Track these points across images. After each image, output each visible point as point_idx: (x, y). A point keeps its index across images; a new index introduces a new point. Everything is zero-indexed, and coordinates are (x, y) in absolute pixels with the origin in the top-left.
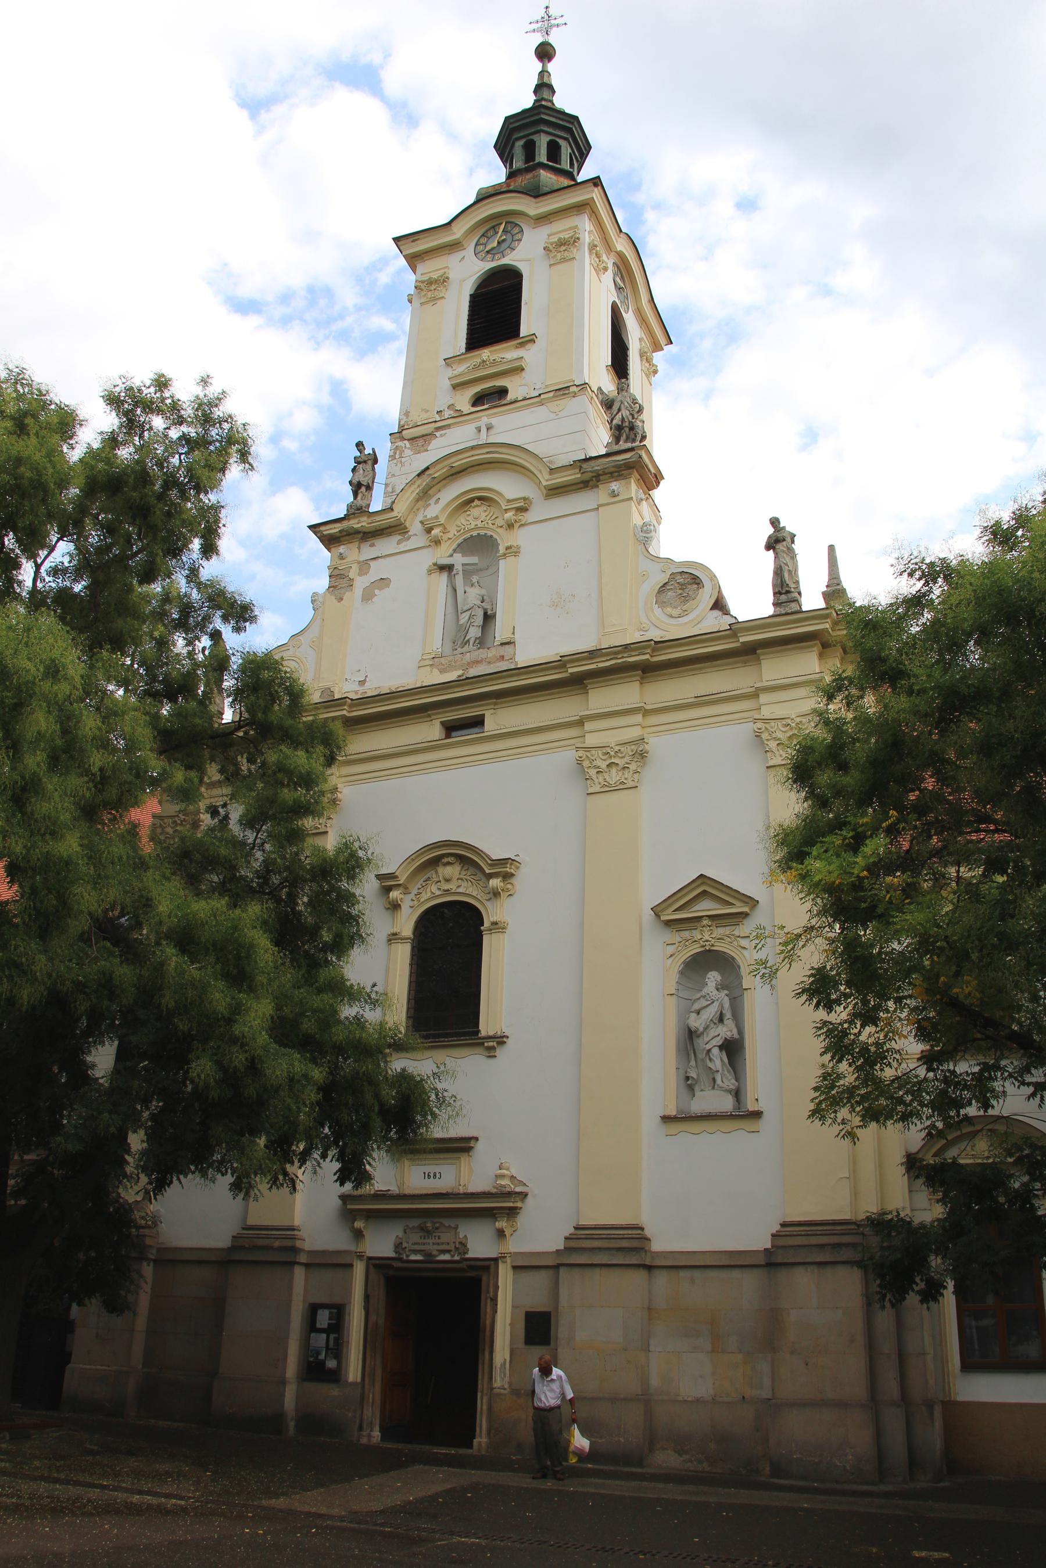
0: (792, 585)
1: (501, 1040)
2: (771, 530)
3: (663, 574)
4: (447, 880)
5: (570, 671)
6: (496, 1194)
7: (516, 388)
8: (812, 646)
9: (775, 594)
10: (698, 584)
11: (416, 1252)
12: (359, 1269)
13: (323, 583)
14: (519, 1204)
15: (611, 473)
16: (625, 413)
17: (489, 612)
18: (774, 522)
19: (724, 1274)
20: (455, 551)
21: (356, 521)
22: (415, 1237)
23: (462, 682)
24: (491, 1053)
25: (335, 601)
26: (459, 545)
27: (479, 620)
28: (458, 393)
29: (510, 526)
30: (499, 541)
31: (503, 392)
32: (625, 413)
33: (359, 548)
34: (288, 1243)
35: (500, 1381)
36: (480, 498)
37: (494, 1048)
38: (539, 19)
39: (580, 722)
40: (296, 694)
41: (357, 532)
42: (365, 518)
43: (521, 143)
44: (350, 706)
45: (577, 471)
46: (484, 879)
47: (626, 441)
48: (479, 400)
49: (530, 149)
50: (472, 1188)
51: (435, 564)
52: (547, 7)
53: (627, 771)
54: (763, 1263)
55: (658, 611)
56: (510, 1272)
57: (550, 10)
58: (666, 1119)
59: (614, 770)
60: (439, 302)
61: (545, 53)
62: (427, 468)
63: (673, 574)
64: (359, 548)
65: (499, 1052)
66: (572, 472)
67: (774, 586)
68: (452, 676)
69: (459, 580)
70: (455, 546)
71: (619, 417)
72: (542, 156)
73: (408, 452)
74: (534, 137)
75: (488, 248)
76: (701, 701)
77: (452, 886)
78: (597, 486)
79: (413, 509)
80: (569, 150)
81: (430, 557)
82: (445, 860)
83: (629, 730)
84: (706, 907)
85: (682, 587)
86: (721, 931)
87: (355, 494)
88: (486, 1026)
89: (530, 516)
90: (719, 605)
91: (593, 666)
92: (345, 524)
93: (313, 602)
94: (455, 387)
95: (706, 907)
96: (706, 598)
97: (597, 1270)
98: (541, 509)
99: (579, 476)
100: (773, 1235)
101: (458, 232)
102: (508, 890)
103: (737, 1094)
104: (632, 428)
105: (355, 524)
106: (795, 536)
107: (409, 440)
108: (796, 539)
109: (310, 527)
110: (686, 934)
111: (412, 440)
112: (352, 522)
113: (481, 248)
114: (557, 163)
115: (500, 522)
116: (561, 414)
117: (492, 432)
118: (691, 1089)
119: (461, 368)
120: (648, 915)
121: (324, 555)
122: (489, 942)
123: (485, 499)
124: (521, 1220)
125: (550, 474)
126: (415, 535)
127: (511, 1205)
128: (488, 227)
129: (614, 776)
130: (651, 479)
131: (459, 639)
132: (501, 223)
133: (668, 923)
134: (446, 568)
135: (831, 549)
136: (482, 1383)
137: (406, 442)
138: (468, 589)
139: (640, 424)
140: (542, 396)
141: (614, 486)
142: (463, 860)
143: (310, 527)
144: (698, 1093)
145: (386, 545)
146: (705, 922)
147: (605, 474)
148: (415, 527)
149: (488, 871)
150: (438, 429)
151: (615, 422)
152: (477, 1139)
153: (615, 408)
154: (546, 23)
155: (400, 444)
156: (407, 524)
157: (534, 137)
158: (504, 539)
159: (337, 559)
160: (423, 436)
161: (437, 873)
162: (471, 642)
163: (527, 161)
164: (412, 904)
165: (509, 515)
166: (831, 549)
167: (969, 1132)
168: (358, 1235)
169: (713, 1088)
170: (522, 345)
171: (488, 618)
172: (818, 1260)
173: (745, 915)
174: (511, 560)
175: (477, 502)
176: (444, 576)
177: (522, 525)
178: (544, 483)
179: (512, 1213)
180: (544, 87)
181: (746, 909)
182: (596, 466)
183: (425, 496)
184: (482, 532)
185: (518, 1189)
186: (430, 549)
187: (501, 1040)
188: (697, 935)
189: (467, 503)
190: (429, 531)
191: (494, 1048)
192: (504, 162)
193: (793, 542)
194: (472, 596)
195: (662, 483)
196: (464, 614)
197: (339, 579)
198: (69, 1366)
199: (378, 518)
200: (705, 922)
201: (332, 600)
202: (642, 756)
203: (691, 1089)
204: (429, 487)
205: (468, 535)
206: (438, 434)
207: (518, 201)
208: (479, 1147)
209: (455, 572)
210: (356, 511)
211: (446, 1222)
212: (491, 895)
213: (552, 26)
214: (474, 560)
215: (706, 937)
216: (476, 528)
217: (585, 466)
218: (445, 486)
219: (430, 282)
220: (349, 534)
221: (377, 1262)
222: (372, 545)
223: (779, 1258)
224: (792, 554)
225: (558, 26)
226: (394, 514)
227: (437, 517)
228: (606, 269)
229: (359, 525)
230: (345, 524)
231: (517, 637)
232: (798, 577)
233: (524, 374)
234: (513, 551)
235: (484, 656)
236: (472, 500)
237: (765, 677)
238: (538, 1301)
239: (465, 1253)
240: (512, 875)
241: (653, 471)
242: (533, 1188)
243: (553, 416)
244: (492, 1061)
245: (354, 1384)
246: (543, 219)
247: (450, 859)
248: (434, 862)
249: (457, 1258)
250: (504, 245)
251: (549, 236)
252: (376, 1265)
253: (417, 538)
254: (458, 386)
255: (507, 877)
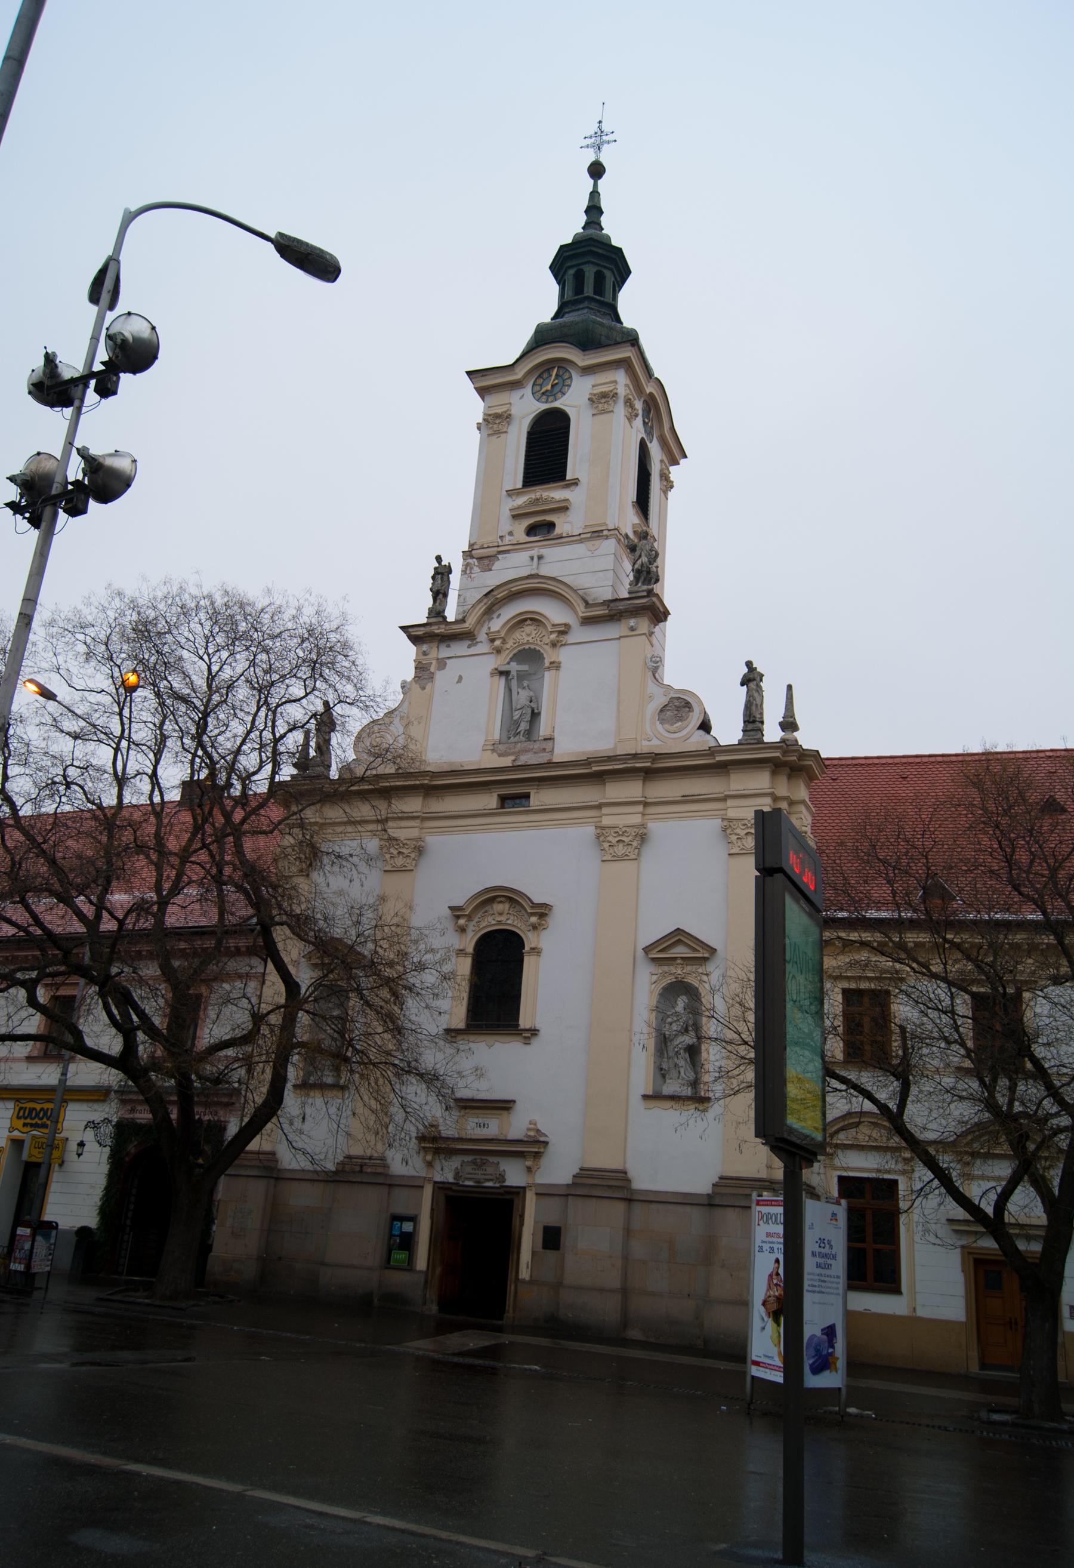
0: (758, 716)
1: (534, 1032)
2: (746, 670)
3: (665, 698)
4: (501, 914)
5: (594, 769)
6: (527, 1141)
7: (564, 525)
8: (766, 767)
9: (744, 722)
10: (689, 708)
11: (470, 1179)
12: (428, 1191)
13: (409, 674)
14: (542, 1150)
15: (631, 612)
16: (644, 559)
17: (536, 711)
18: (749, 664)
19: (679, 1208)
20: (511, 659)
21: (437, 627)
22: (469, 1169)
23: (514, 768)
24: (527, 1041)
25: (419, 689)
26: (515, 655)
27: (528, 717)
28: (517, 522)
29: (554, 645)
30: (545, 656)
31: (551, 526)
32: (644, 559)
33: (438, 648)
34: (380, 1170)
35: (524, 1274)
36: (531, 619)
37: (528, 1038)
38: (593, 133)
39: (599, 807)
40: (252, 605)
41: (437, 635)
42: (443, 626)
43: (572, 272)
44: (431, 777)
45: (606, 607)
46: (526, 916)
47: (643, 584)
48: (531, 530)
49: (579, 277)
50: (510, 1137)
51: (496, 669)
52: (600, 122)
53: (630, 847)
54: (706, 1203)
55: (659, 727)
56: (534, 1197)
57: (603, 124)
58: (646, 1097)
59: (621, 845)
60: (503, 436)
61: (596, 171)
62: (492, 590)
63: (672, 698)
64: (438, 648)
65: (535, 1041)
66: (602, 608)
67: (745, 715)
68: (507, 761)
69: (514, 683)
70: (511, 655)
71: (639, 562)
72: (589, 290)
73: (476, 569)
74: (583, 267)
75: (544, 390)
76: (687, 800)
77: (502, 918)
78: (620, 620)
79: (480, 622)
80: (613, 279)
81: (492, 662)
82: (499, 899)
83: (632, 818)
84: (680, 951)
85: (678, 708)
86: (689, 968)
87: (435, 599)
88: (524, 1022)
89: (570, 638)
90: (705, 726)
91: (610, 767)
92: (428, 629)
93: (403, 687)
94: (515, 517)
95: (680, 951)
96: (695, 720)
97: (594, 1200)
98: (579, 634)
99: (607, 612)
100: (713, 1185)
101: (519, 374)
102: (543, 925)
103: (695, 1084)
104: (649, 572)
105: (436, 630)
106: (763, 675)
107: (477, 559)
108: (764, 678)
109: (401, 628)
110: (666, 968)
111: (480, 559)
112: (433, 628)
113: (538, 388)
114: (601, 296)
115: (546, 640)
116: (596, 553)
117: (542, 561)
118: (664, 1076)
119: (521, 501)
120: (640, 953)
121: (410, 650)
122: (528, 962)
123: (534, 620)
124: (544, 1161)
125: (586, 608)
126: (481, 642)
127: (536, 1150)
128: (541, 371)
129: (620, 850)
130: (659, 614)
131: (511, 728)
132: (554, 367)
133: (654, 960)
134: (505, 674)
135: (790, 688)
136: (512, 1276)
137: (475, 560)
138: (520, 690)
139: (654, 569)
140: (582, 536)
141: (632, 622)
142: (510, 899)
143: (401, 628)
144: (668, 1081)
145: (459, 648)
146: (679, 961)
147: (626, 612)
148: (482, 636)
149: (529, 911)
150: (500, 552)
151: (636, 566)
152: (514, 1101)
153: (637, 553)
154: (599, 138)
155: (470, 561)
156: (476, 633)
157: (583, 267)
158: (549, 655)
159: (420, 654)
160: (488, 557)
161: (492, 908)
162: (522, 733)
163: (576, 294)
164: (474, 928)
165: (553, 636)
166: (790, 688)
167: (853, 1123)
168: (430, 1164)
169: (678, 1078)
170: (568, 486)
171: (535, 715)
172: (742, 1205)
173: (705, 959)
174: (553, 672)
175: (529, 622)
176: (503, 680)
177: (562, 645)
178: (581, 615)
179: (537, 1155)
180: (594, 210)
181: (706, 955)
182: (621, 606)
183: (490, 612)
184: (533, 647)
185: (542, 1139)
186: (492, 656)
187: (534, 1032)
188: (673, 969)
189: (521, 621)
190: (492, 641)
191: (528, 1038)
192: (559, 283)
193: (761, 680)
194: (522, 697)
195: (669, 617)
196: (517, 712)
197: (421, 669)
198: (212, 1254)
199: (454, 627)
200: (679, 961)
201: (416, 688)
202: (643, 838)
203: (664, 1076)
204: (493, 605)
205: (522, 648)
206: (500, 556)
207: (570, 350)
208: (518, 1106)
209: (511, 677)
210: (437, 613)
211: (492, 1159)
212: (531, 928)
213: (603, 143)
214: (525, 667)
215: (679, 972)
216: (528, 643)
217: (612, 605)
218: (504, 604)
219: (497, 416)
220: (430, 636)
221: (441, 1185)
222: (448, 646)
223: (717, 1201)
224: (759, 690)
225: (609, 142)
226: (466, 625)
227: (498, 632)
228: (637, 415)
229: (439, 631)
230: (428, 629)
231: (556, 735)
232: (762, 709)
233: (568, 513)
234: (556, 666)
235: (531, 747)
236: (525, 620)
237: (732, 788)
238: (553, 1220)
239: (504, 1182)
240: (547, 914)
241: (662, 610)
242: (552, 1139)
243: (589, 554)
244: (528, 1047)
245: (420, 1272)
246: (588, 370)
247: (501, 899)
248: (492, 900)
249: (497, 1185)
250: (557, 389)
251: (593, 386)
252: (440, 1187)
253: (483, 647)
254: (515, 517)
255: (542, 916)
